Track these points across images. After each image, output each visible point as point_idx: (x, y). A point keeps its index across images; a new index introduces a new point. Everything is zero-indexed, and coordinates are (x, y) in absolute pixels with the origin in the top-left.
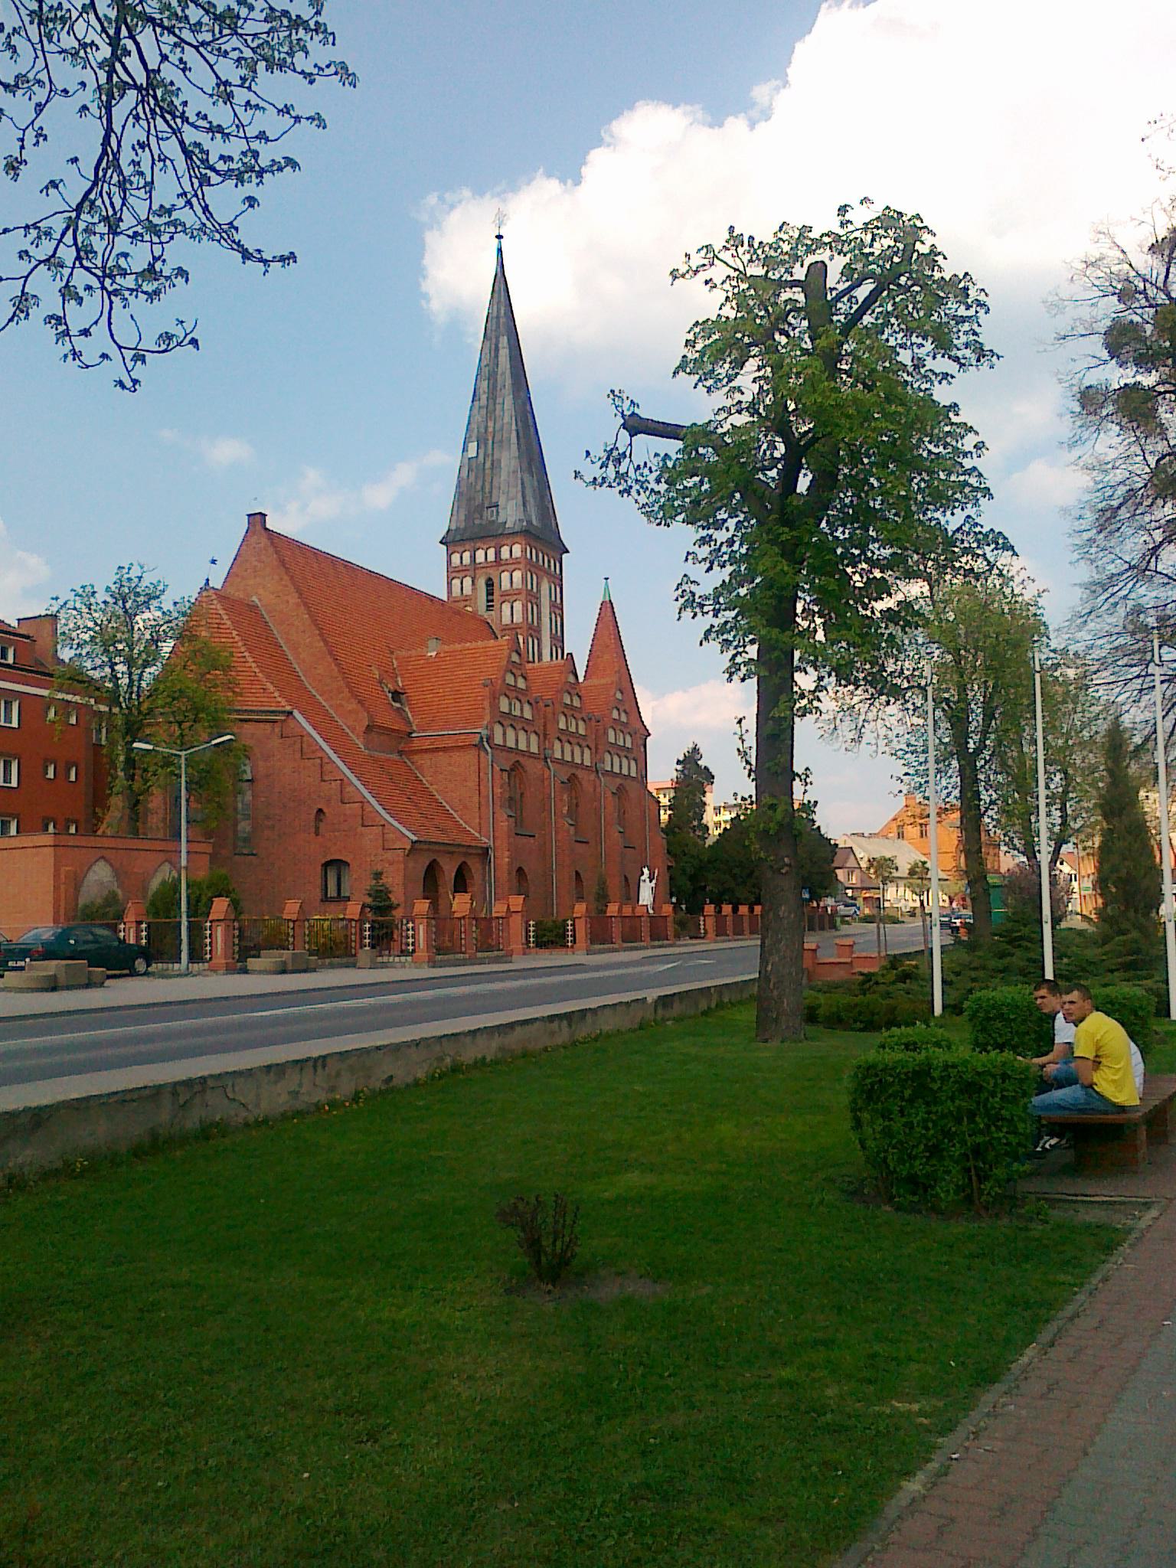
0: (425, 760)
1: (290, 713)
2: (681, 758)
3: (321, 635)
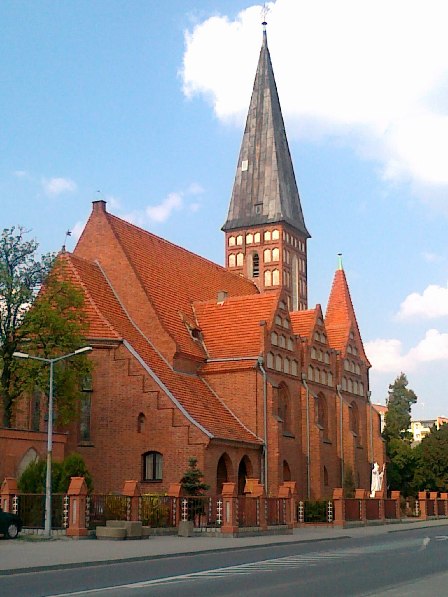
0: (216, 379)
1: (121, 342)
2: (393, 384)
3: (143, 287)
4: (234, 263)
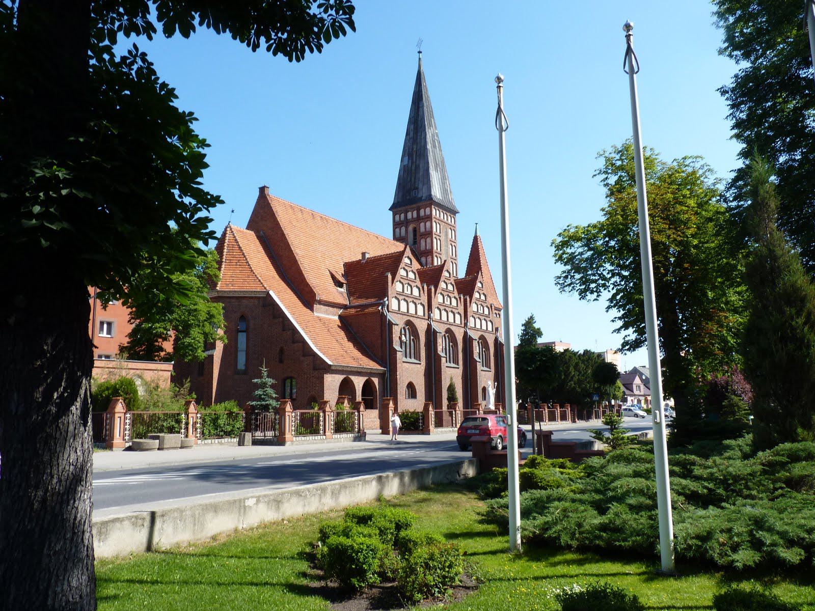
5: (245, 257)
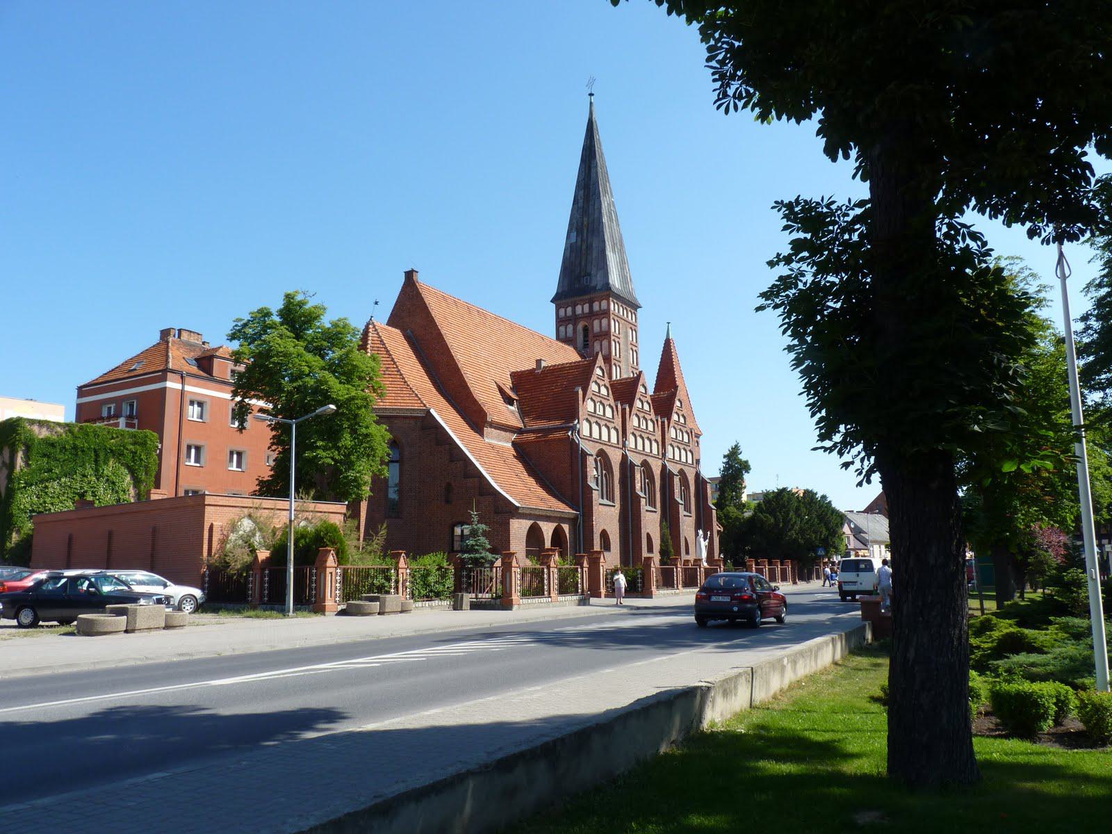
4: (564, 334)
5: (395, 363)
